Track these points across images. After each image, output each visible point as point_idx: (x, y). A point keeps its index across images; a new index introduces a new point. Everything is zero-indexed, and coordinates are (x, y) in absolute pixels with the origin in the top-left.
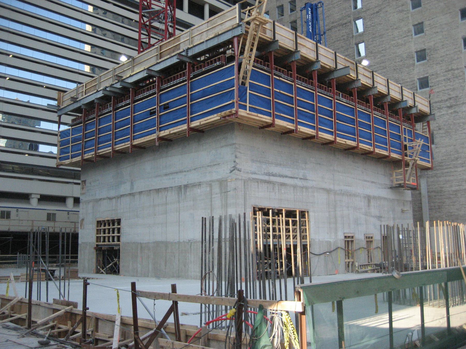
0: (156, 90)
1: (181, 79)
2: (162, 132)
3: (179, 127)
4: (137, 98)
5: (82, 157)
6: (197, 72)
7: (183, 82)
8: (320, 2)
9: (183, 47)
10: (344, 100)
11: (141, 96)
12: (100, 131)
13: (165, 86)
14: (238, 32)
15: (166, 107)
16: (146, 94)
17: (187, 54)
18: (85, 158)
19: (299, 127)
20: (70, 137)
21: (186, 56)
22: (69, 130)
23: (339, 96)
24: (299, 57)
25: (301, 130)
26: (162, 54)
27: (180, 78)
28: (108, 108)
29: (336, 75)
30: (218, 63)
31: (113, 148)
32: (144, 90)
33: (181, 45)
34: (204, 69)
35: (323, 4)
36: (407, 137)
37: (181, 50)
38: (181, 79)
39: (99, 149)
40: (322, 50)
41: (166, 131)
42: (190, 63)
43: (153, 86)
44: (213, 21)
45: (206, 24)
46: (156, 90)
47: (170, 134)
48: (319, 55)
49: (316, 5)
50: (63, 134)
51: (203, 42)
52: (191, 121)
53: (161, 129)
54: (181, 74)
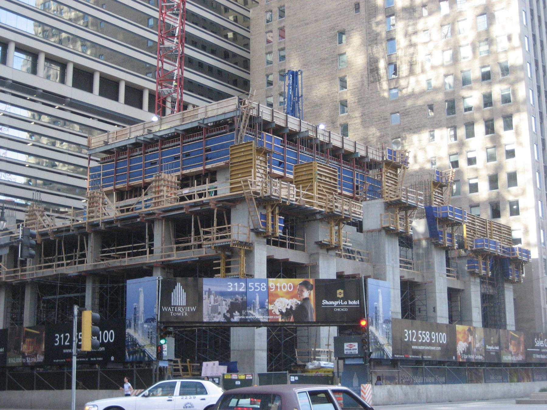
0: (180, 142)
1: (199, 137)
2: (185, 171)
3: (197, 168)
4: (163, 147)
5: (114, 187)
6: (210, 134)
7: (200, 139)
8: (300, 71)
9: (201, 117)
10: (308, 153)
11: (166, 146)
12: (131, 168)
13: (187, 141)
14: (238, 113)
15: (188, 155)
16: (171, 145)
17: (203, 122)
18: (116, 188)
19: (273, 170)
20: (102, 172)
21: (203, 123)
22: (100, 166)
23: (304, 150)
24: (274, 126)
25: (274, 172)
26: (185, 119)
27: (198, 136)
28: (137, 151)
29: (301, 136)
30: (224, 131)
31: (143, 181)
32: (169, 142)
33: (199, 115)
34: (214, 133)
35: (302, 72)
36: (359, 180)
37: (199, 119)
38: (199, 137)
39: (130, 181)
40: (291, 118)
41: (188, 170)
42: (205, 128)
43: (177, 139)
44: (221, 104)
45: (217, 105)
46: (180, 142)
47: (190, 173)
48: (288, 123)
49: (297, 73)
50: (93, 169)
51: (215, 116)
52: (206, 165)
53: (183, 169)
54: (198, 134)
